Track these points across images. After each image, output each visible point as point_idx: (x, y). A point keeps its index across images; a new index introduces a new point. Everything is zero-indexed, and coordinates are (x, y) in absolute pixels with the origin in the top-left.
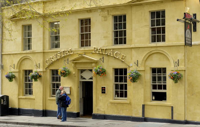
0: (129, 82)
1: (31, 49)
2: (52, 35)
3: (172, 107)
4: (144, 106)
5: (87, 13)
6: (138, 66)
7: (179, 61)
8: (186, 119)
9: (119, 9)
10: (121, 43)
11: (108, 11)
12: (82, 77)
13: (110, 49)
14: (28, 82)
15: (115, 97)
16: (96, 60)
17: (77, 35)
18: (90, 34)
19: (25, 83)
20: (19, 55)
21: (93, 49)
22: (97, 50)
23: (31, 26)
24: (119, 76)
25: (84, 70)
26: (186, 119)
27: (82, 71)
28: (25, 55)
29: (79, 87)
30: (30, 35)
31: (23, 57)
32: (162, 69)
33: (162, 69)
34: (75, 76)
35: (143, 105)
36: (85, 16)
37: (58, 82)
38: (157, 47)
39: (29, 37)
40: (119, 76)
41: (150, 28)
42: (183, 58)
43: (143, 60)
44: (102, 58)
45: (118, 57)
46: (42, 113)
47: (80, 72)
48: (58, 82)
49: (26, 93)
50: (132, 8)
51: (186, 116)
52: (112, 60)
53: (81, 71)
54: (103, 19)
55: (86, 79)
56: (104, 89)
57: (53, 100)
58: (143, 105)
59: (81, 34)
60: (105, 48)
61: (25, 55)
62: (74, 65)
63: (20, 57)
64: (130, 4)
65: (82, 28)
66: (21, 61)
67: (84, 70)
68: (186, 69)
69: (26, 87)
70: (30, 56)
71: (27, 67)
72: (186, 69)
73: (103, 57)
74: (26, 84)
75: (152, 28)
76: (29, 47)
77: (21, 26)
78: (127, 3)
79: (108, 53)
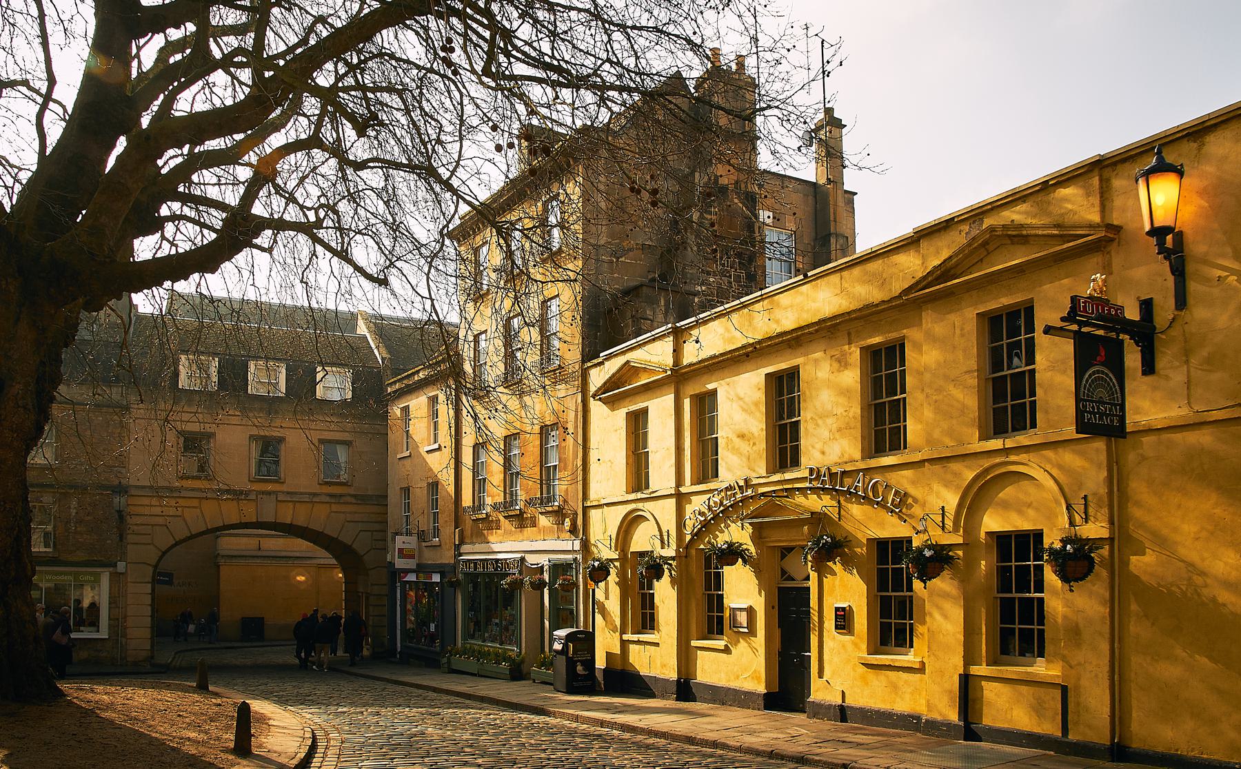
2: (875, 399)
5: (790, 350)
6: (943, 529)
9: (881, 321)
10: (1019, 427)
11: (849, 334)
12: (783, 572)
13: (858, 471)
14: (713, 592)
15: (657, 645)
17: (762, 429)
20: (620, 507)
21: (806, 474)
24: (1013, 564)
28: (633, 506)
31: (987, 471)
32: (1013, 537)
33: (1013, 537)
37: (651, 592)
42: (1103, 491)
45: (880, 499)
46: (761, 702)
47: (778, 554)
48: (651, 592)
49: (710, 631)
50: (923, 313)
53: (782, 552)
54: (836, 365)
55: (794, 580)
56: (843, 613)
59: (993, 379)
61: (633, 506)
63: (623, 510)
64: (913, 295)
67: (790, 549)
68: (1116, 535)
70: (648, 506)
72: (1116, 535)
78: (900, 296)
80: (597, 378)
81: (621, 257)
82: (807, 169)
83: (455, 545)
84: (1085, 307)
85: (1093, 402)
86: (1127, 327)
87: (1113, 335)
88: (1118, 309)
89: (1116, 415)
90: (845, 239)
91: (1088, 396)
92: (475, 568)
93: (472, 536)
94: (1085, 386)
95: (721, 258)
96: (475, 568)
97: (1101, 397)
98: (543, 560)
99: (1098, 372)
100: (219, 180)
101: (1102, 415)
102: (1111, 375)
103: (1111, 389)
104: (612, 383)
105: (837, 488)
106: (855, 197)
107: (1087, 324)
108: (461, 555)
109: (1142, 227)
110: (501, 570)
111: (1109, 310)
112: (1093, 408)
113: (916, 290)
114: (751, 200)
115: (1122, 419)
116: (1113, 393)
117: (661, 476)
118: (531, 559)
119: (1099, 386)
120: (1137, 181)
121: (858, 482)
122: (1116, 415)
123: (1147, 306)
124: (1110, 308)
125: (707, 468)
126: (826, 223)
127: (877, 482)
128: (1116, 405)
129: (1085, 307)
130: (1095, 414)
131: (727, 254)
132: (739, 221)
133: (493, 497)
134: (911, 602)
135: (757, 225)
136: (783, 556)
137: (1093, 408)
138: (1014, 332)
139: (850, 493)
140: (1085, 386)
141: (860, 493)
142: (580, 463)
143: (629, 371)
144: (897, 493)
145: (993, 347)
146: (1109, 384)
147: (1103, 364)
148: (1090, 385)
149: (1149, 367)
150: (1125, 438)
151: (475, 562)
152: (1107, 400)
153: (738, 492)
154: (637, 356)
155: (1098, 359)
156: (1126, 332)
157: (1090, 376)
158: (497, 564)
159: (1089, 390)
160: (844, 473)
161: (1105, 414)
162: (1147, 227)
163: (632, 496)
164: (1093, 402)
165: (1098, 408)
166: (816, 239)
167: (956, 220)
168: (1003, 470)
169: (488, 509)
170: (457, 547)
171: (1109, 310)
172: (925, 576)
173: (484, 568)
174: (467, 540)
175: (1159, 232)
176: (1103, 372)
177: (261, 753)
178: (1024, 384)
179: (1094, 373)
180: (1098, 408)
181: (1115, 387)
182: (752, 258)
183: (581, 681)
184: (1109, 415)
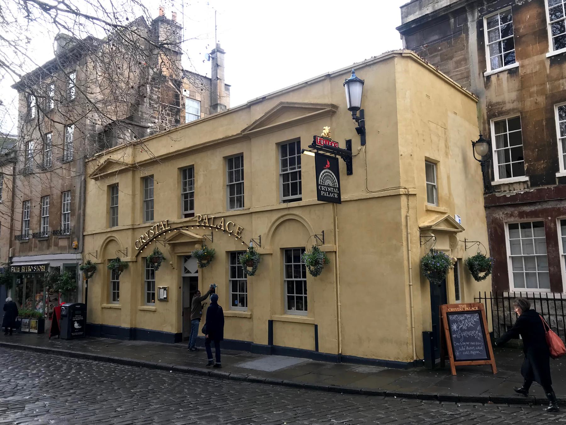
0: (309, 278)
1: (244, 207)
3: (316, 327)
4: (271, 323)
7: (261, 237)
8: (340, 352)
12: (186, 269)
16: (199, 239)
18: (300, 172)
19: (233, 281)
22: (202, 220)
23: (242, 157)
25: (188, 257)
26: (340, 352)
27: (187, 258)
28: (109, 235)
29: (180, 288)
30: (240, 175)
31: (282, 216)
34: (174, 268)
35: (269, 321)
36: (185, 163)
38: (289, 208)
39: (186, 192)
40: (293, 264)
41: (280, 175)
43: (102, 246)
44: (211, 234)
45: (231, 232)
47: (183, 260)
51: (340, 345)
52: (226, 237)
57: (144, 310)
58: (269, 321)
60: (213, 216)
61: (109, 235)
62: (170, 248)
63: (104, 237)
65: (231, 174)
66: (105, 245)
69: (290, 290)
71: (112, 253)
73: (212, 233)
74: (290, 284)
75: (283, 174)
76: (240, 202)
77: (222, 158)
79: (219, 223)
80: (92, 168)
81: (109, 106)
82: (206, 70)
83: (9, 257)
84: (320, 141)
85: (325, 186)
86: (337, 151)
87: (333, 155)
88: (335, 144)
89: (336, 193)
90: (225, 107)
91: (322, 183)
92: (21, 270)
93: (19, 252)
94: (321, 178)
95: (162, 111)
96: (21, 270)
97: (329, 184)
98: (60, 264)
99: (327, 172)
100: (29, 94)
101: (329, 193)
102: (333, 174)
103: (333, 180)
104: (102, 169)
105: (211, 226)
106: (230, 87)
107: (321, 149)
108: (12, 263)
109: (347, 106)
110: (36, 271)
111: (331, 144)
112: (325, 189)
113: (248, 130)
114: (178, 84)
115: (339, 195)
116: (334, 182)
117: (124, 220)
118: (53, 264)
119: (327, 179)
120: (344, 85)
121: (221, 223)
122: (336, 193)
123: (349, 143)
124: (332, 143)
125: (149, 215)
126: (216, 100)
127: (230, 223)
128: (336, 188)
129: (320, 141)
130: (326, 192)
131: (165, 109)
132: (171, 93)
133: (33, 230)
134: (246, 283)
135: (180, 96)
136: (186, 261)
137: (325, 189)
138: (292, 153)
139: (218, 228)
140: (321, 178)
141: (222, 228)
142: (81, 212)
143: (109, 163)
144: (239, 228)
145: (283, 160)
146: (332, 178)
147: (329, 169)
148: (323, 178)
149: (350, 171)
150: (341, 203)
151: (20, 266)
152: (331, 185)
153: (163, 228)
154: (116, 157)
155: (327, 166)
156: (339, 155)
157: (323, 174)
158: (33, 268)
159: (323, 181)
160: (214, 218)
161: (331, 192)
162: (348, 107)
163: (109, 230)
164: (325, 186)
165: (328, 189)
166: (211, 106)
167: (267, 98)
168: (291, 217)
169: (31, 237)
170: (11, 258)
171: (331, 144)
172: (479, 257)
173: (25, 270)
174: (16, 255)
175: (353, 109)
176: (329, 173)
177: (114, 340)
178: (297, 175)
179: (325, 172)
180: (328, 189)
181: (335, 179)
182: (179, 111)
183: (77, 332)
184: (333, 192)
